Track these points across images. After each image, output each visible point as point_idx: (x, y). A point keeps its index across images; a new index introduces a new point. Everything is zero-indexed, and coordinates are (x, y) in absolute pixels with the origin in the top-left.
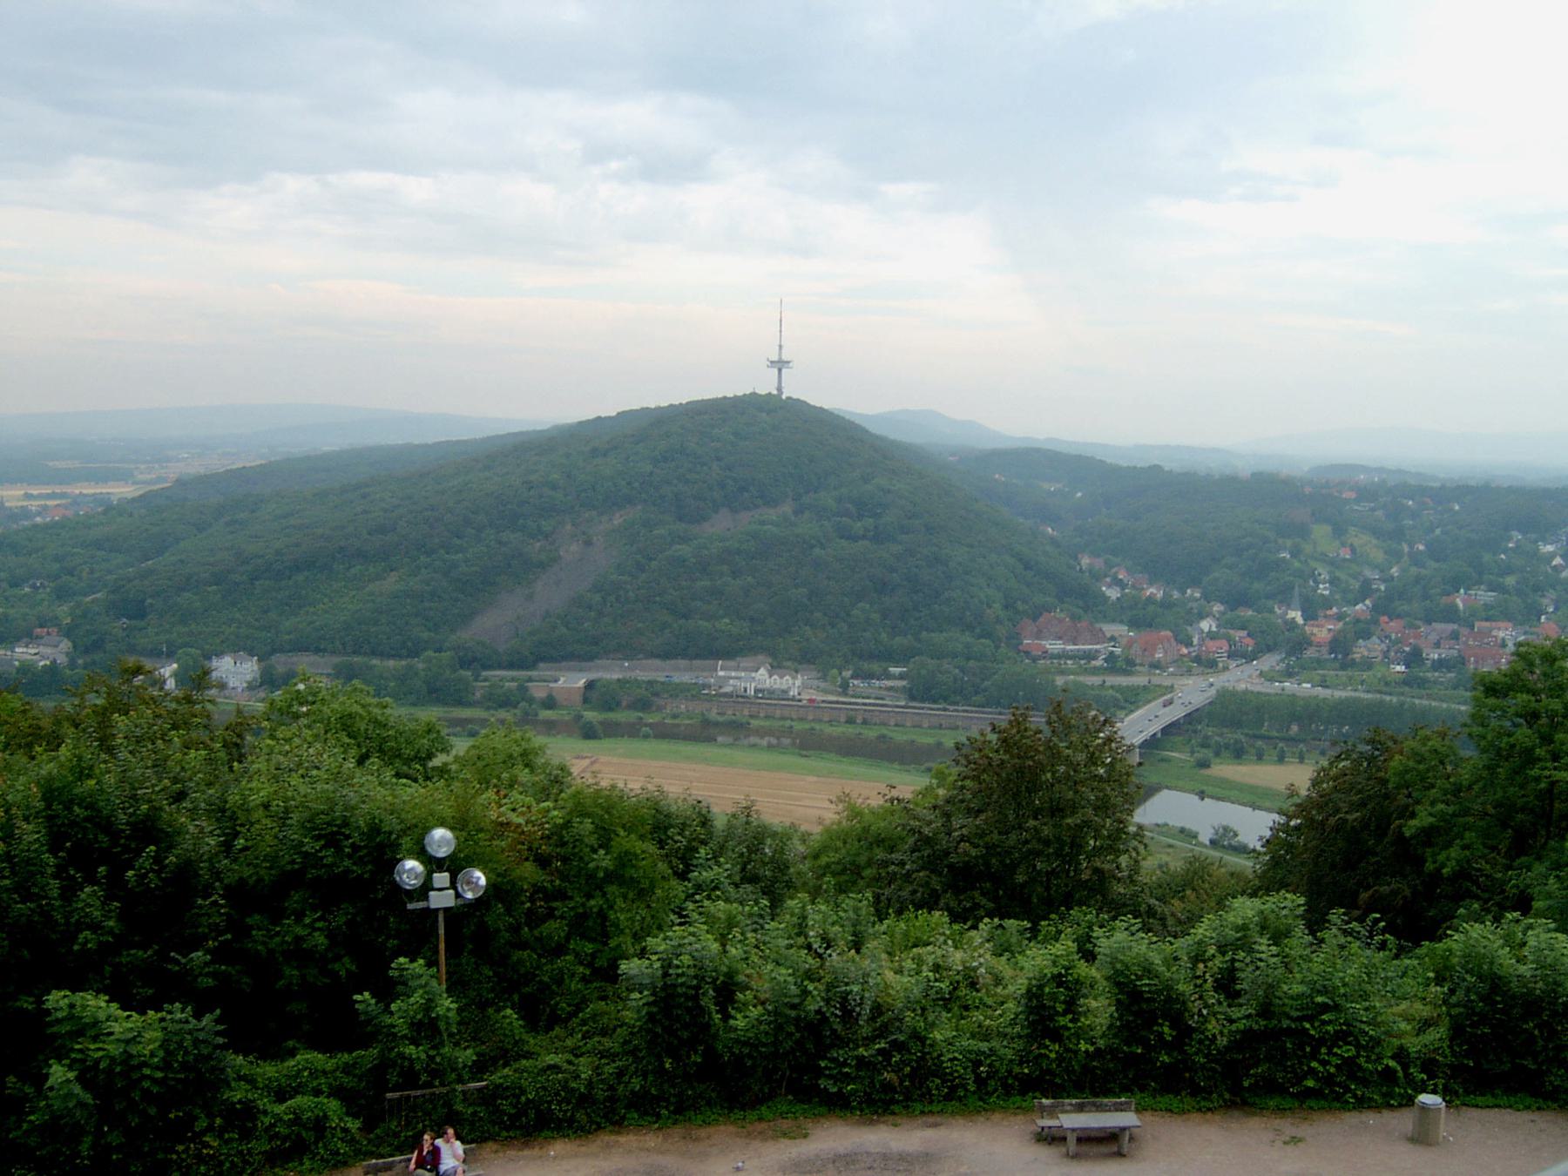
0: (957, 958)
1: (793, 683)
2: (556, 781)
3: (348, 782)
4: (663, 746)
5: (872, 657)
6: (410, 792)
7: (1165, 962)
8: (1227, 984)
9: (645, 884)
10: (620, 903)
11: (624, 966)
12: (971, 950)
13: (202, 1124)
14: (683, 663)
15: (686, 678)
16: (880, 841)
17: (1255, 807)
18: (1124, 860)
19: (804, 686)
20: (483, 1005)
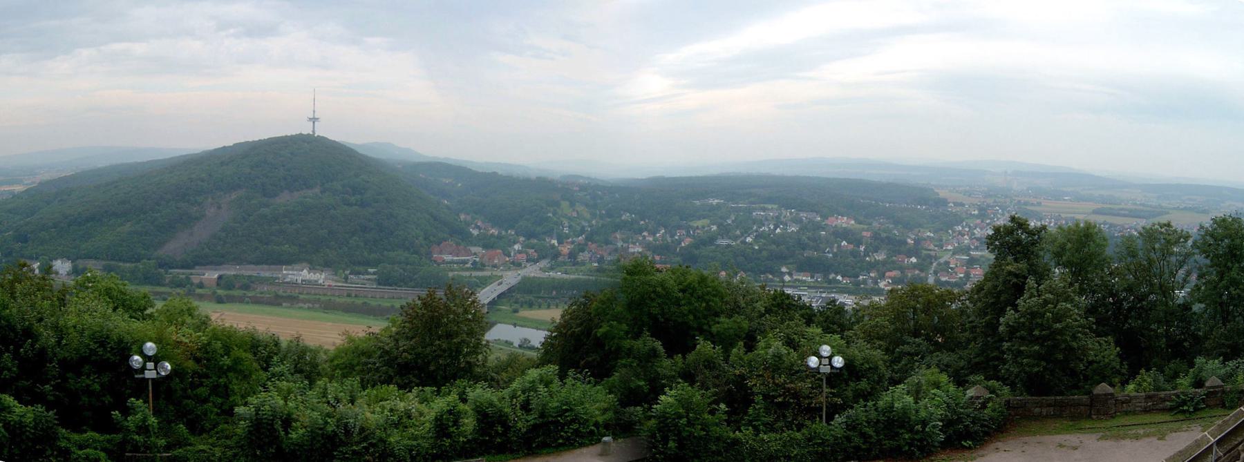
0: (401, 406)
1: (320, 277)
2: (204, 323)
3: (109, 319)
4: (256, 307)
5: (360, 263)
6: (136, 325)
7: (500, 400)
8: (526, 407)
9: (247, 373)
10: (235, 381)
11: (236, 409)
12: (409, 402)
13: (49, 452)
14: (266, 267)
15: (267, 274)
16: (363, 353)
17: (537, 329)
18: (480, 357)
19: (326, 279)
20: (169, 422)
